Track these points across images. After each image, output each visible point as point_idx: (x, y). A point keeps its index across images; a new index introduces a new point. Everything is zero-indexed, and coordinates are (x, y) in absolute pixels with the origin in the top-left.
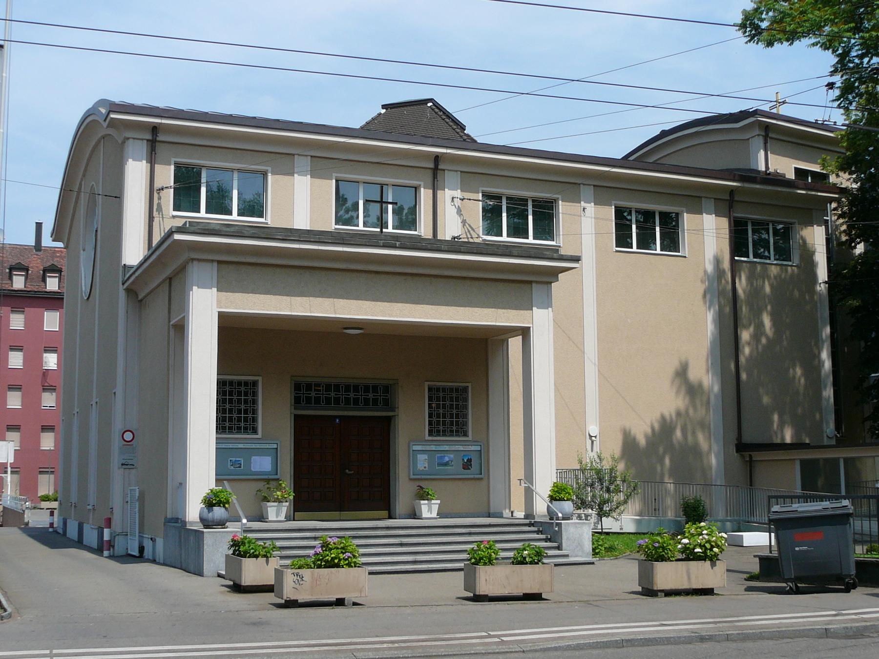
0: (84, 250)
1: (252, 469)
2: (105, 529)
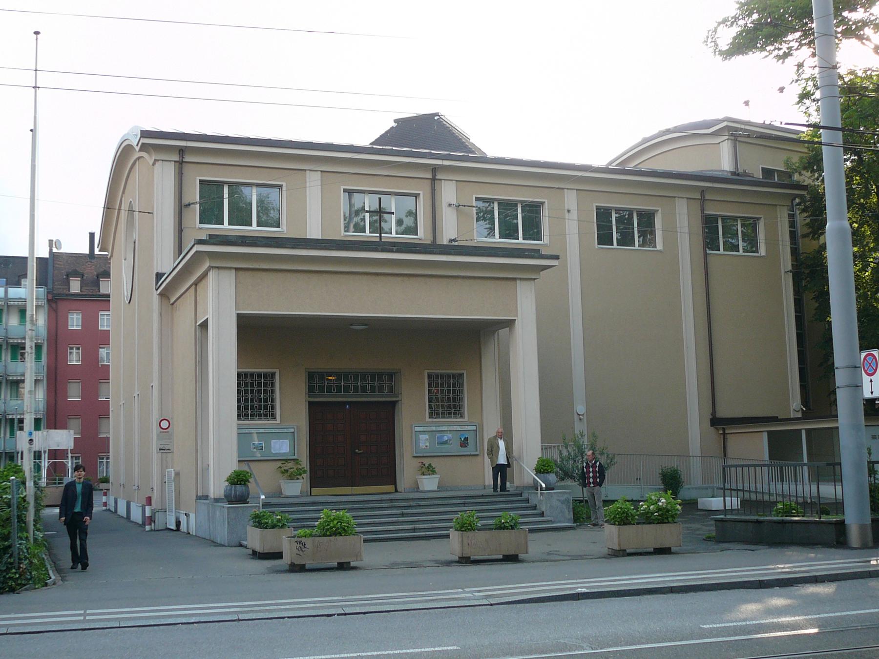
0: (125, 260)
1: (272, 450)
2: (146, 507)
